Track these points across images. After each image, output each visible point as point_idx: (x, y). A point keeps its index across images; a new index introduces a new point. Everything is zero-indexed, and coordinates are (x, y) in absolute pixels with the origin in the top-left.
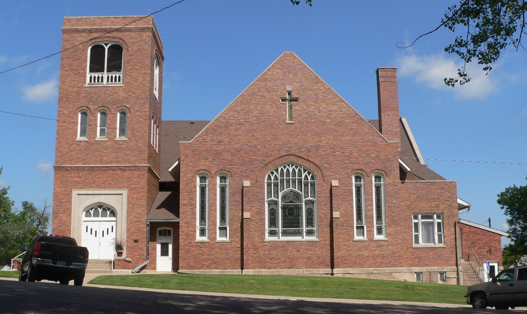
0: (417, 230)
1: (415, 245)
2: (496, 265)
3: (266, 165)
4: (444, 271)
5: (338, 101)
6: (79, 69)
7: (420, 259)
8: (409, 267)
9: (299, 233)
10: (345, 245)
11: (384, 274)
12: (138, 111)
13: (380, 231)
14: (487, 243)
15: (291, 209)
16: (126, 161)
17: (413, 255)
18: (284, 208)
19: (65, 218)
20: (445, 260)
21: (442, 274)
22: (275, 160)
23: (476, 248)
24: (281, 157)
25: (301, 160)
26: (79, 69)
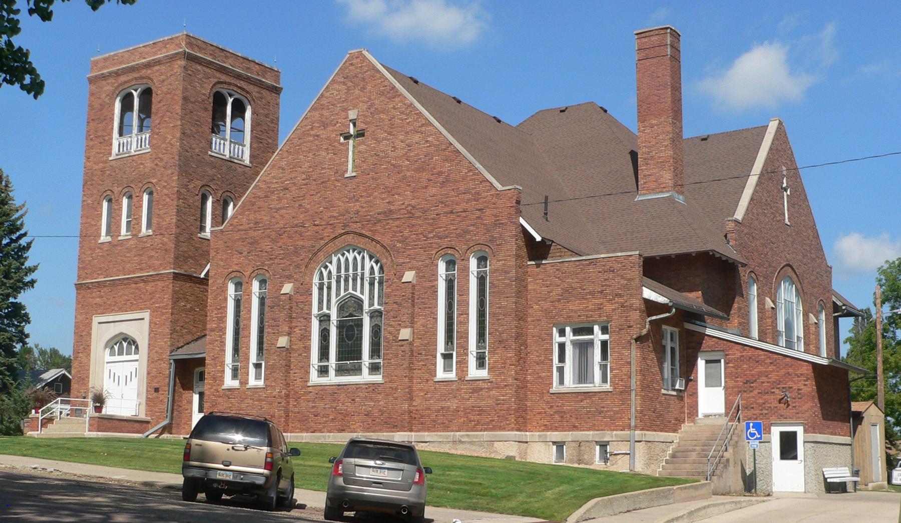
0: (562, 358)
1: (555, 387)
2: (800, 430)
3: (315, 254)
4: (606, 439)
5: (423, 125)
6: (104, 134)
7: (562, 414)
8: (543, 430)
9: (357, 370)
10: (421, 390)
11: (480, 444)
12: (164, 187)
13: (481, 363)
15: (351, 328)
16: (150, 267)
17: (552, 407)
18: (341, 326)
19: (84, 360)
20: (611, 417)
21: (603, 445)
22: (327, 244)
23: (756, 392)
24: (335, 238)
25: (363, 240)
26: (104, 134)
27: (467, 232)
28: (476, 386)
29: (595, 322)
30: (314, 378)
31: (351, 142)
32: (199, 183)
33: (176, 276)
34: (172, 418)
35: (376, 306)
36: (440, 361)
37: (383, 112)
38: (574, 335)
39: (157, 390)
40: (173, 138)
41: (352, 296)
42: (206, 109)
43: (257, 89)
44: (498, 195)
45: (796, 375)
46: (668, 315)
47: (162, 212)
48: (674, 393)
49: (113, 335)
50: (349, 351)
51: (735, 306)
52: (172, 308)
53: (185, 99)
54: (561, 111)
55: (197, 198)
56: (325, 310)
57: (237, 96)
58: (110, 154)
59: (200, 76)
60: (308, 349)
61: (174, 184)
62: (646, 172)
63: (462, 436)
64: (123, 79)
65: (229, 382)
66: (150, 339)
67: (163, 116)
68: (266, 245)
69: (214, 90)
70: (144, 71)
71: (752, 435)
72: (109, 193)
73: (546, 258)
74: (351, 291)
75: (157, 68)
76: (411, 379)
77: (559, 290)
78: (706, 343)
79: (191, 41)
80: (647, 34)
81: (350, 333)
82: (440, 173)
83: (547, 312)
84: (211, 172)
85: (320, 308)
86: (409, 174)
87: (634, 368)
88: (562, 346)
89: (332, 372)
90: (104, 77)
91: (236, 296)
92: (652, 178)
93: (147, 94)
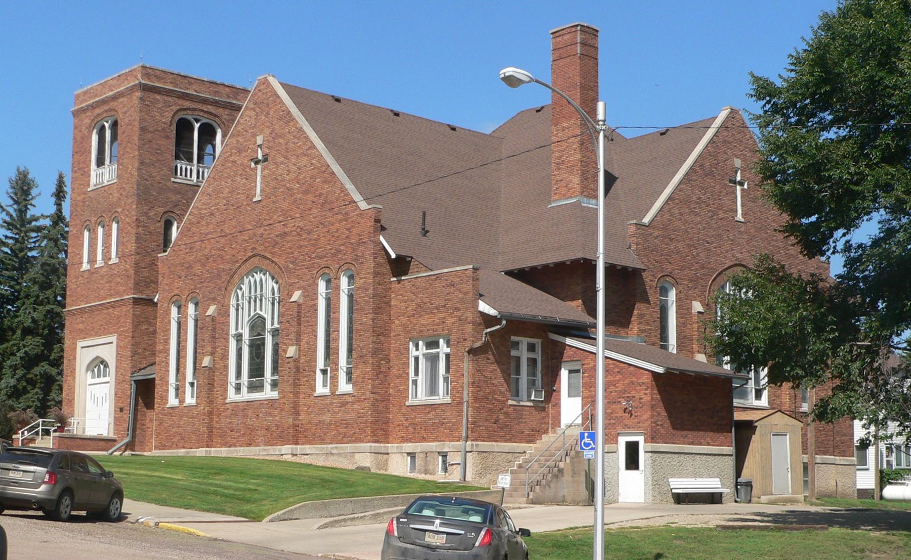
1: (410, 401)
2: (641, 439)
8: (401, 442)
10: (305, 405)
12: (127, 216)
14: (625, 391)
21: (444, 455)
24: (246, 260)
27: (339, 251)
28: (343, 401)
29: (440, 336)
30: (232, 396)
31: (259, 167)
32: (162, 210)
33: (136, 301)
34: (134, 436)
35: (276, 325)
36: (319, 376)
37: (281, 137)
38: (427, 349)
39: (121, 410)
40: (133, 167)
41: (260, 317)
42: (168, 137)
43: (227, 112)
44: (362, 214)
45: (638, 383)
46: (499, 327)
47: (125, 240)
48: (531, 404)
49: (91, 359)
51: (636, 312)
52: (133, 332)
53: (143, 129)
54: (538, 111)
55: (158, 224)
56: (240, 330)
57: (204, 121)
58: (89, 185)
59: (160, 105)
60: (226, 367)
61: (133, 213)
62: (559, 178)
63: (332, 448)
64: (98, 111)
65: (173, 401)
66: (117, 361)
67: (125, 147)
68: (197, 269)
69: (177, 118)
70: (112, 104)
71: (587, 445)
72: (88, 223)
73: (406, 274)
74: (258, 311)
75: (121, 100)
76: (296, 394)
77: (413, 306)
78: (568, 353)
79: (147, 71)
80: (561, 33)
82: (320, 195)
83: (404, 326)
84: (174, 198)
85: (237, 329)
86: (298, 196)
87: (466, 380)
88: (417, 359)
89: (244, 389)
90: (83, 110)
92: (563, 184)
93: (115, 125)
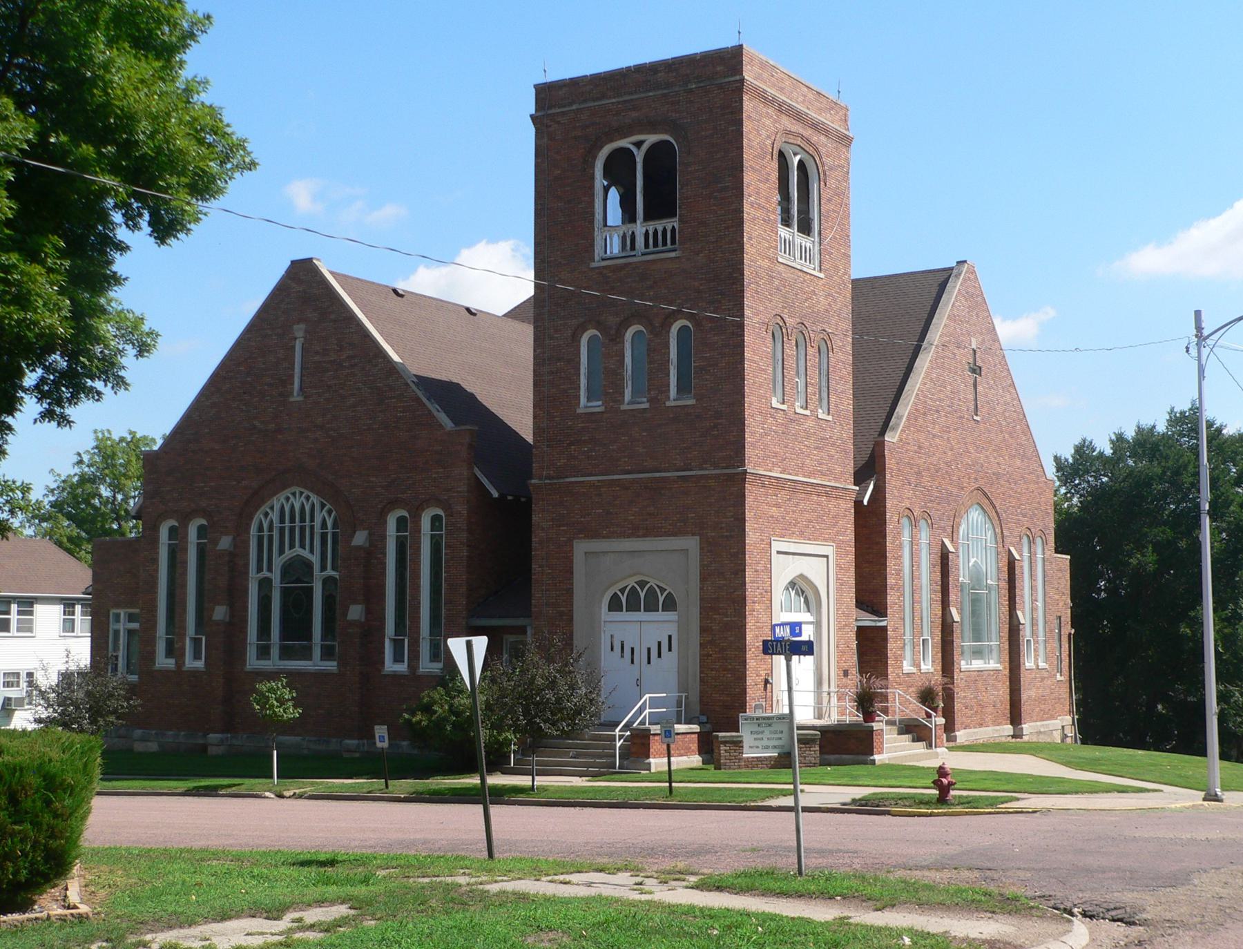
9: (306, 654)
18: (285, 592)
27: (1034, 515)
35: (330, 572)
39: (846, 673)
50: (296, 627)
56: (265, 573)
81: (297, 604)
85: (260, 569)
89: (275, 652)
91: (198, 544)
